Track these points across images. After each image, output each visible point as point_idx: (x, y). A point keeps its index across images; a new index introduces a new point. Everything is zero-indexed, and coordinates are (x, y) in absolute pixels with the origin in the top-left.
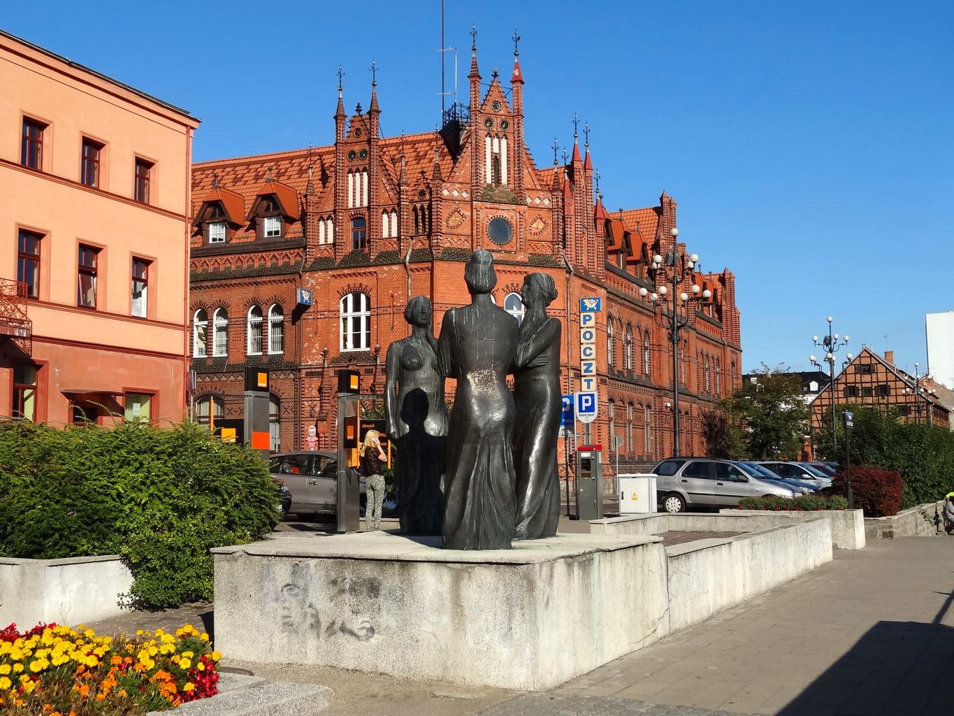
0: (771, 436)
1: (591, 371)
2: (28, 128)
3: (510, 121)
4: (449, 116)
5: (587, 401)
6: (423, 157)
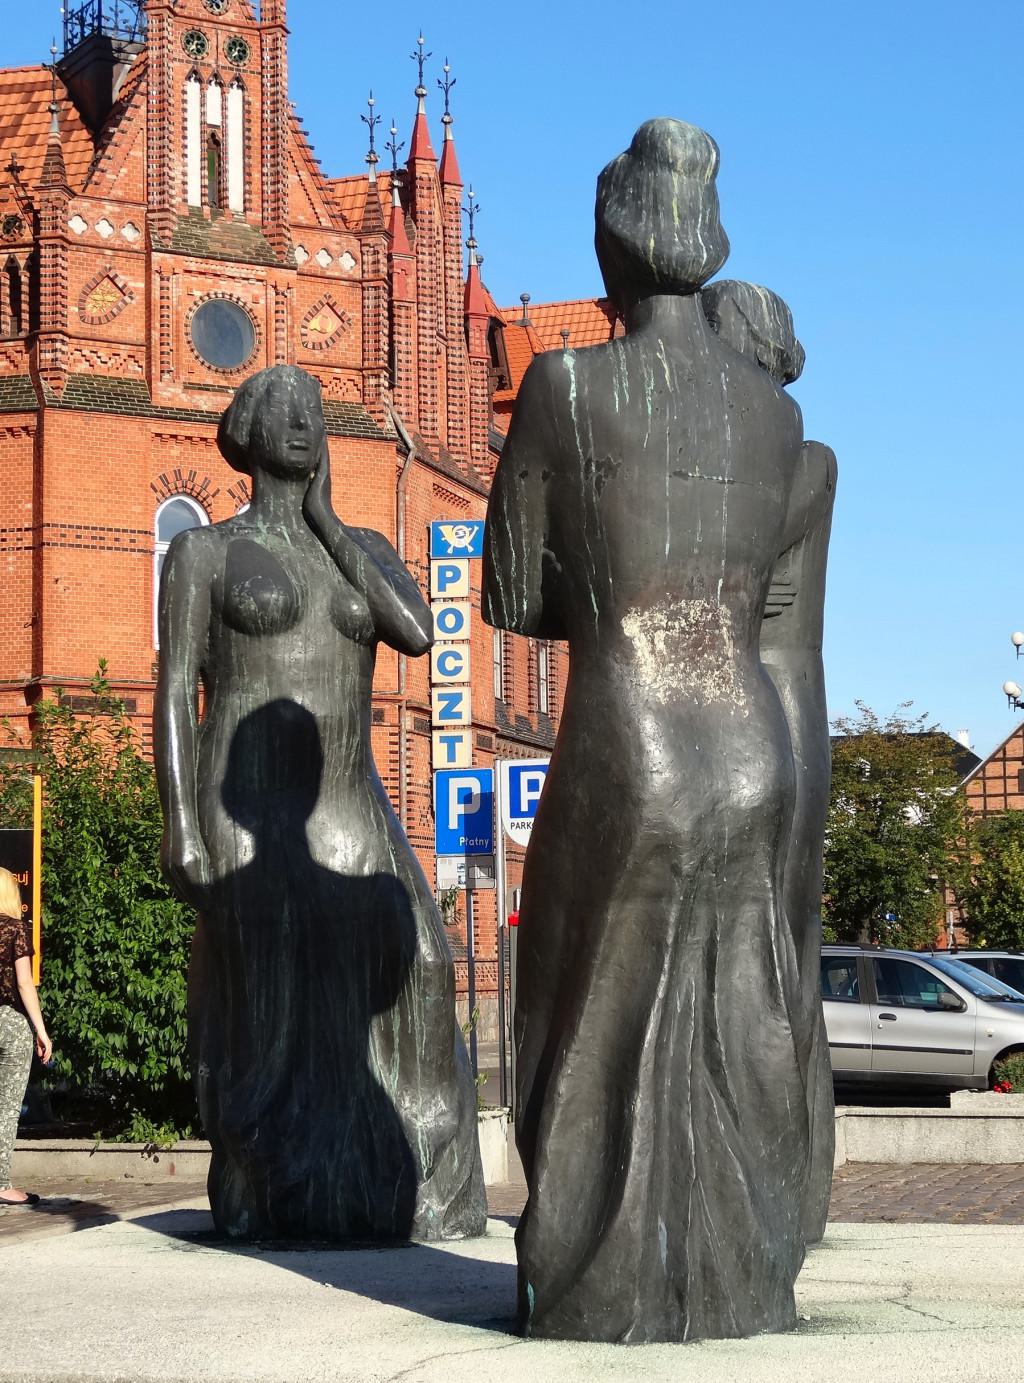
0: (882, 888)
1: (459, 715)
3: (253, 43)
4: (82, 25)
6: (10, 132)
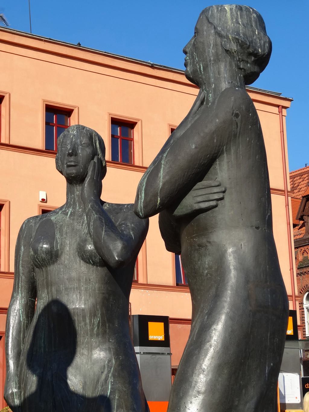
2: (119, 129)
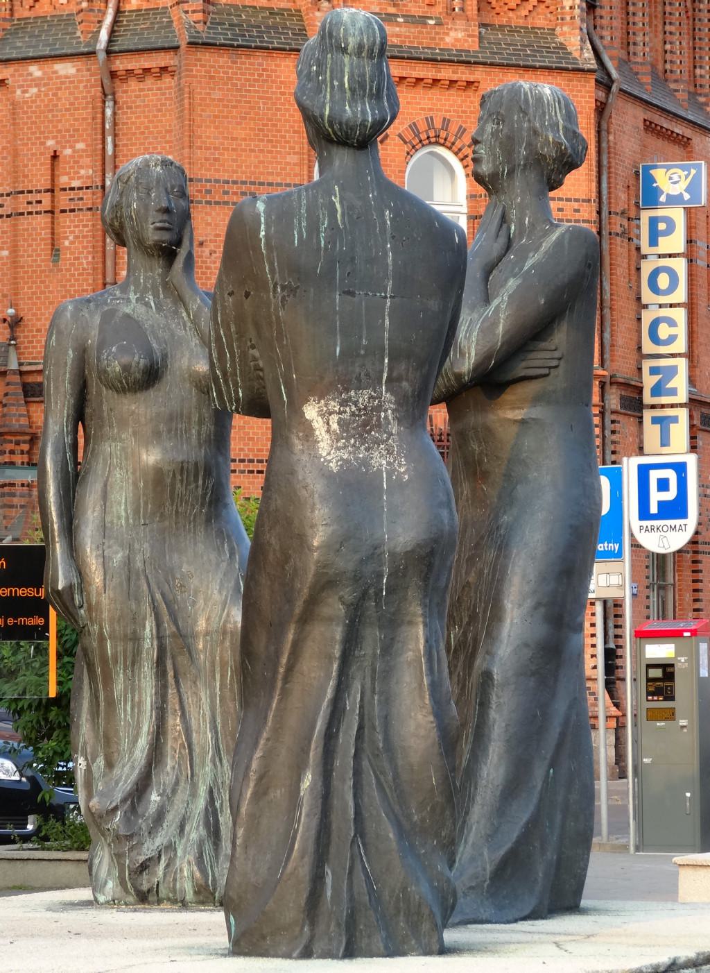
1: (674, 392)
5: (663, 485)
